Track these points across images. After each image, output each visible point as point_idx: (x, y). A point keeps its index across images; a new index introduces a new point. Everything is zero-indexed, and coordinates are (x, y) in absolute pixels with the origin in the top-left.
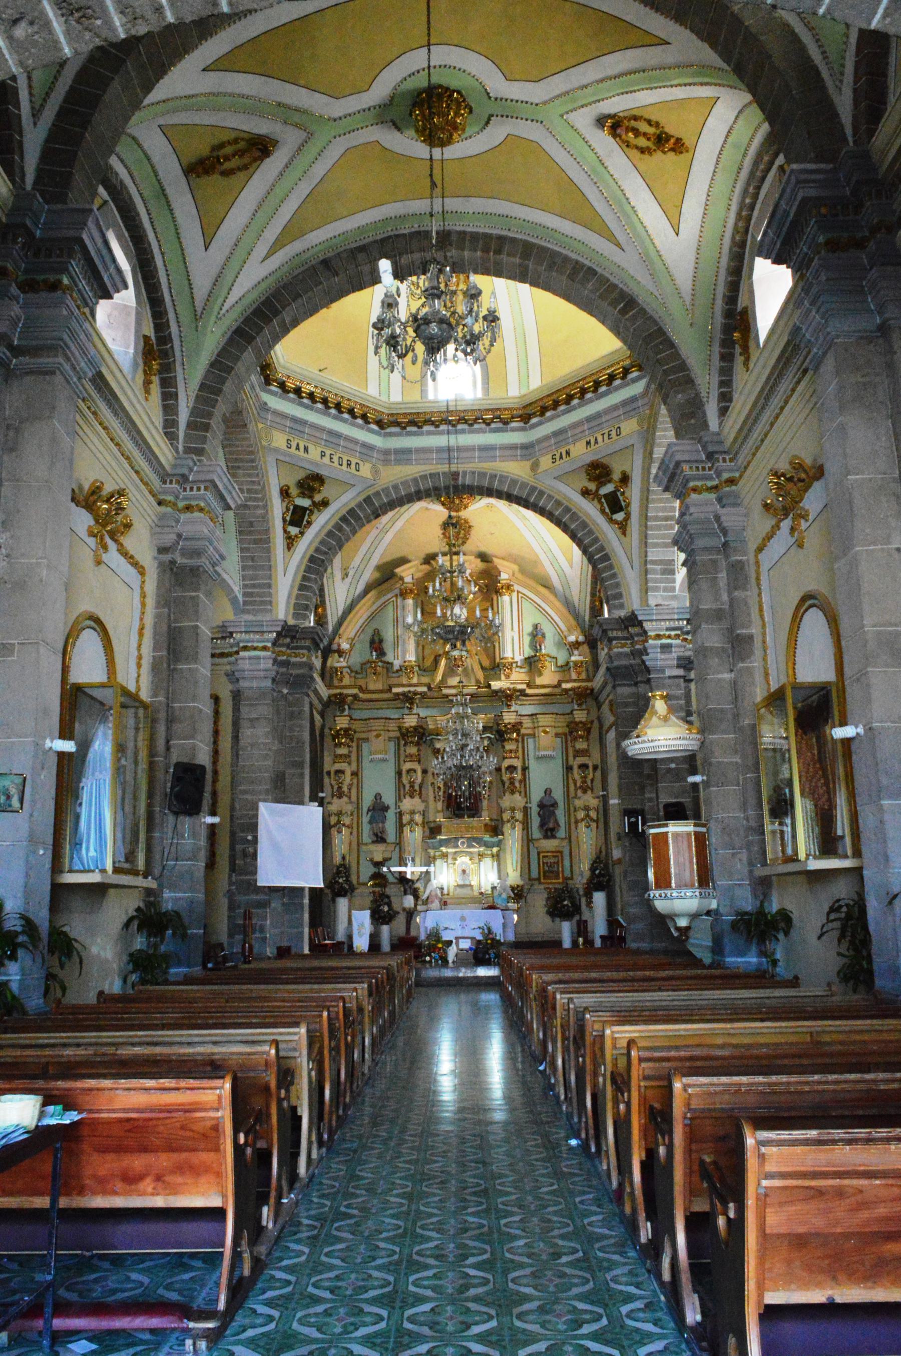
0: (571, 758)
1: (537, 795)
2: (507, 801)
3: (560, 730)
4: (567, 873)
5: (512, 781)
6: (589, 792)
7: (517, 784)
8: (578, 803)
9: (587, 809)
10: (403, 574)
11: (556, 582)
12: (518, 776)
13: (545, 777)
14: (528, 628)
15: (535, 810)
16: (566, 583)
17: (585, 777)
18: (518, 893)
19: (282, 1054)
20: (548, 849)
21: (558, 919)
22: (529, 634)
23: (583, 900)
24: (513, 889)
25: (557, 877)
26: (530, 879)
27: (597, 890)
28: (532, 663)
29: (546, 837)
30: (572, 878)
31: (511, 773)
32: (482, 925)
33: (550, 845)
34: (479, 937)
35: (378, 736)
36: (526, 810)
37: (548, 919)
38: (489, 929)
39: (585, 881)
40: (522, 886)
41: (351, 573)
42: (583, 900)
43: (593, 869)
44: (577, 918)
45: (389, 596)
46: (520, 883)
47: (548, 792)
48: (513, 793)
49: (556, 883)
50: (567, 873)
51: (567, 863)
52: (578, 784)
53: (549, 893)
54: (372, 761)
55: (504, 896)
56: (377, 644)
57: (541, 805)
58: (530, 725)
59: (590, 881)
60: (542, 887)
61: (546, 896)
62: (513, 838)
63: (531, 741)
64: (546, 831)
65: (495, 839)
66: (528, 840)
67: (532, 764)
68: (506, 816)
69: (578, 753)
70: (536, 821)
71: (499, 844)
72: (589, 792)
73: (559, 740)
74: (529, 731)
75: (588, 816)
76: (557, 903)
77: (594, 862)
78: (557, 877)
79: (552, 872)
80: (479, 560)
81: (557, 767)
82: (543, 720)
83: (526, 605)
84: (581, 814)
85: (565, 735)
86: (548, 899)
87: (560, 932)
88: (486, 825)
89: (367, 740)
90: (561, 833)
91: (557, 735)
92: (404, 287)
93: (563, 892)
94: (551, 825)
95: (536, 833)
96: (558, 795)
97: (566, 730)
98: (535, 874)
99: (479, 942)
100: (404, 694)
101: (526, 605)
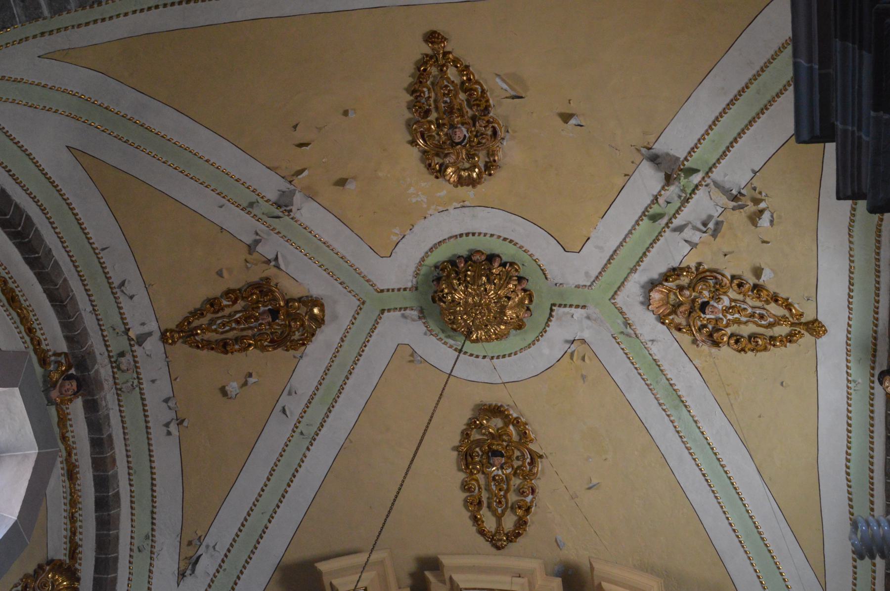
41: (207, 565)
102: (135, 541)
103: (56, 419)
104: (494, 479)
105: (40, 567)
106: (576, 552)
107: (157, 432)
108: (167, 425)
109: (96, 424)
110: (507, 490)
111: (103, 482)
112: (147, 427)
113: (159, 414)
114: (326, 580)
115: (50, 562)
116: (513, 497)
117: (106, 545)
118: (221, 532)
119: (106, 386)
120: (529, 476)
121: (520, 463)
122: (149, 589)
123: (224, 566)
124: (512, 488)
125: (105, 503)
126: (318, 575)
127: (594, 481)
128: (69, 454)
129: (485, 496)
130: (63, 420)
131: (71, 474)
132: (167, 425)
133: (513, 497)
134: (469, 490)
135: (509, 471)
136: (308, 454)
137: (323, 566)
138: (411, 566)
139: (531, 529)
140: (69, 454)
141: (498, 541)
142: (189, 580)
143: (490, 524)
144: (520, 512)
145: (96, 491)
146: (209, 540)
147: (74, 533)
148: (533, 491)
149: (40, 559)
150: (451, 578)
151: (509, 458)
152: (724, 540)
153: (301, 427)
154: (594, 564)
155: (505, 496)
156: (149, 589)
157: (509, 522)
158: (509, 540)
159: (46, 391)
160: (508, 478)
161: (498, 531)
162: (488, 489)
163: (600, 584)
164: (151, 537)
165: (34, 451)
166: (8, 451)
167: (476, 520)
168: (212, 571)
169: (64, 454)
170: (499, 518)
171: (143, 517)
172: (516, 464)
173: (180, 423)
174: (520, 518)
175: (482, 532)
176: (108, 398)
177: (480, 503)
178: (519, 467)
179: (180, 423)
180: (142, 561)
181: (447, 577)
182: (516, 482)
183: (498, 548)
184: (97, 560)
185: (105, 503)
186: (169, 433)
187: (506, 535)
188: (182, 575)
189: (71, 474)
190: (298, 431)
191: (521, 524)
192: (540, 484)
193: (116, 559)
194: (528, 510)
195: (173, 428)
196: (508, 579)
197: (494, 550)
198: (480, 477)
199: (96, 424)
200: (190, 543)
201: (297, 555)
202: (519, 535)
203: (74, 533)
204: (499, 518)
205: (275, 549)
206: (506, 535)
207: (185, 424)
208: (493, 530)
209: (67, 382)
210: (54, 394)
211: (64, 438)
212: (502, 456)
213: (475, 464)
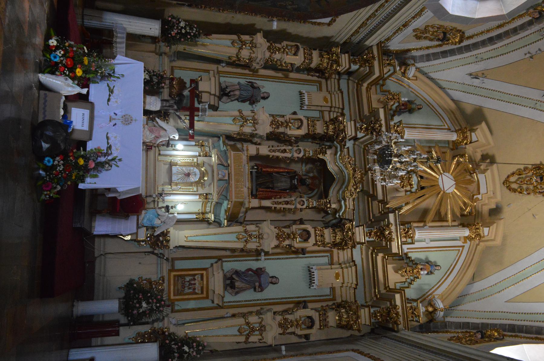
0: (318, 305)
1: (272, 266)
2: (269, 230)
3: (338, 292)
4: (180, 305)
5: (291, 236)
6: (280, 331)
7: (287, 242)
8: (268, 318)
9: (262, 329)
10: (478, 132)
11: (478, 286)
12: (298, 244)
13: (288, 275)
14: (433, 257)
15: (255, 265)
16: (482, 296)
17: (297, 325)
18: (158, 241)
19: (97, 240)
20: (211, 280)
21: (122, 294)
22: (427, 258)
23: (145, 328)
24: (165, 234)
25: (177, 293)
26: (173, 260)
27: (161, 348)
28: (405, 261)
29: (225, 278)
30: (173, 311)
31: (301, 236)
32: (115, 153)
33: (217, 283)
34: (90, 146)
35: (325, 99)
36: (258, 253)
37: (124, 281)
38: (100, 166)
39: (173, 329)
40: (167, 247)
41: (476, 82)
42: (145, 328)
43: (189, 341)
44: (123, 320)
45: (448, 122)
46: (172, 245)
47: (274, 281)
48: (278, 237)
49: (169, 290)
50: (180, 305)
51: (192, 304)
52: (290, 317)
53: (157, 283)
54: (301, 93)
55: (157, 222)
56: (408, 108)
57: (259, 272)
58: (341, 260)
59: (172, 337)
60: (165, 274)
61: (154, 278)
62: (226, 237)
63: (326, 260)
64: (231, 278)
65: (223, 216)
66: (218, 255)
67: (301, 262)
68: (251, 228)
69: (323, 312)
70: (242, 265)
71: (218, 223)
72: (280, 331)
73: (328, 292)
74: (335, 259)
75: (253, 330)
76: (144, 292)
77: (199, 344)
78: (177, 293)
79: (183, 287)
80: (494, 206)
81: (300, 290)
82: (349, 275)
83: (453, 254)
84: (253, 319)
85: (334, 299)
86: (149, 281)
87: (106, 297)
88: (242, 204)
89: (320, 89)
90: (229, 298)
91: (333, 289)
92: (428, 225)
93: (160, 301)
94: (237, 284)
95: (230, 266)
96: (271, 292)
97: (339, 300)
98: (179, 265)
99: (83, 144)
100: (378, 120)
101: (453, 254)
102: (479, 55)
103: (521, 14)
104: (531, 179)
105: (461, 31)
106: (507, 212)
107: (525, 50)
108: (529, 53)
109: (523, 27)
110: (527, 184)
111: (499, 37)
112: (526, 46)
113: (533, 49)
114: (478, 127)
115: (463, 33)
116: (525, 186)
117: (476, 46)
118: (489, 84)
119: (540, 25)
120: (534, 192)
121: (539, 188)
122: (543, 314)
123: (477, 88)
124: (528, 186)
125: (491, 40)
126: (480, 123)
127: (537, 217)
128: (507, 23)
129: (524, 176)
130: (521, 16)
131: (499, 27)
132: (529, 53)
133: (525, 186)
134: (525, 170)
135: (535, 184)
136: (528, 108)
137: (483, 124)
138: (490, 153)
139: (513, 194)
140: (507, 23)
141: (506, 182)
142: (469, 77)
143: (512, 179)
144: (519, 190)
145: (496, 36)
146: (485, 80)
147: (477, 35)
148: (528, 194)
149: (463, 29)
150: (488, 169)
151: (541, 184)
152: (520, 265)
153: (539, 103)
154: (502, 220)
155: (524, 184)
156: (543, 322)
157: (514, 186)
158: (507, 187)
159: (532, 7)
160: (532, 184)
161: (510, 182)
162: (526, 177)
163: (495, 223)
164: (482, 59)
165: (505, 13)
166: (503, 3)
167: (513, 174)
168: (474, 84)
169: (507, 21)
170: (515, 182)
171: (490, 55)
172: (539, 187)
173: (531, 57)
174: (516, 190)
175: (508, 177)
176: (536, 27)
177: (520, 175)
178: (537, 188)
179: (531, 57)
180: (473, 59)
181: (489, 168)
182: (531, 187)
183: (503, 183)
184: (469, 45)
185: (491, 40)
186: (526, 54)
187: (509, 186)
188: (471, 75)
189: (499, 27)
190: (537, 102)
191: (515, 191)
192: (532, 196)
193: (471, 51)
194: (520, 193)
195: (528, 55)
196: (492, 189)
197: (502, 182)
198: (531, 173)
199: (523, 27)
200: (483, 74)
201: (487, 114)
202: (510, 190)
203: (477, 35)
204: (515, 182)
205: (487, 104)
206: (509, 186)
207: (531, 59)
208: (510, 180)
209: (537, 13)
210: (531, 10)
211: (514, 19)
212: (541, 181)
213: (536, 171)
